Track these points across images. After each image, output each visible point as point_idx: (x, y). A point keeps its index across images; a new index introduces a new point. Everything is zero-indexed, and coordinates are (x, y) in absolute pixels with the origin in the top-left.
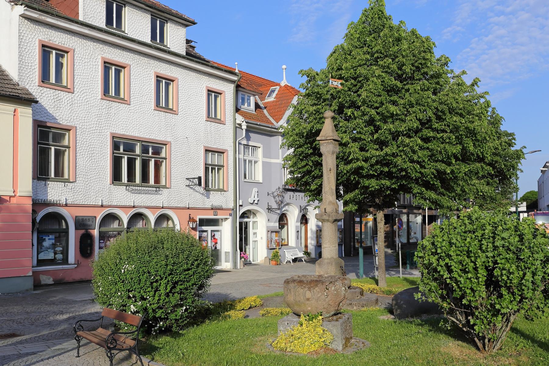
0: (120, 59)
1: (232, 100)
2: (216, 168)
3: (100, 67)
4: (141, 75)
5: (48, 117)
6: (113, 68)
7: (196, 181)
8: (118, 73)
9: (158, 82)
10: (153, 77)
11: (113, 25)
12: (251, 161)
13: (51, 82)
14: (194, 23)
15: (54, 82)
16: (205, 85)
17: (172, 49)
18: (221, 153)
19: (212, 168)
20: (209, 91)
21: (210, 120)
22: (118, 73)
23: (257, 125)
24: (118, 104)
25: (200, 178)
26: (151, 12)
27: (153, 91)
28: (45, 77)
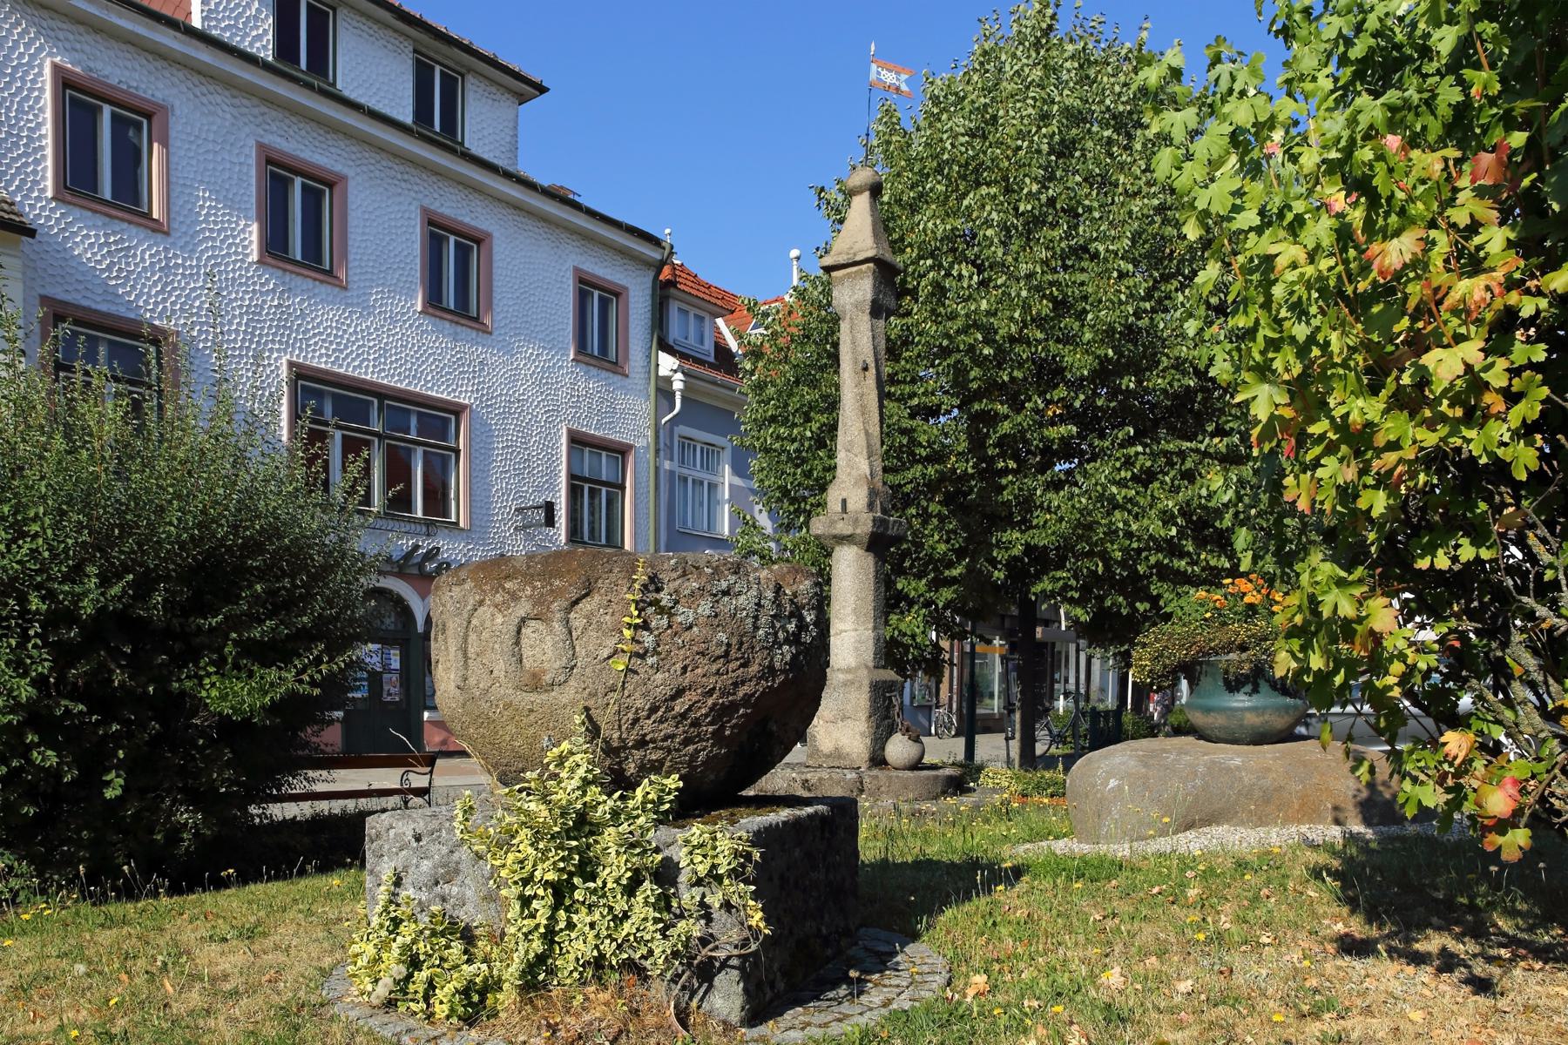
0: (437, 204)
1: (649, 315)
2: (586, 487)
3: (253, 172)
4: (382, 218)
5: (89, 294)
6: (107, 110)
7: (540, 516)
8: (312, 200)
9: (582, 298)
10: (571, 282)
11: (298, 63)
12: (702, 483)
13: (444, 305)
14: (542, 89)
15: (299, 258)
16: (570, 264)
17: (346, 93)
18: (620, 451)
19: (591, 490)
20: (582, 281)
21: (587, 359)
22: (312, 200)
23: (714, 383)
24: (310, 282)
25: (549, 508)
26: (415, 40)
27: (418, 261)
28: (76, 179)
